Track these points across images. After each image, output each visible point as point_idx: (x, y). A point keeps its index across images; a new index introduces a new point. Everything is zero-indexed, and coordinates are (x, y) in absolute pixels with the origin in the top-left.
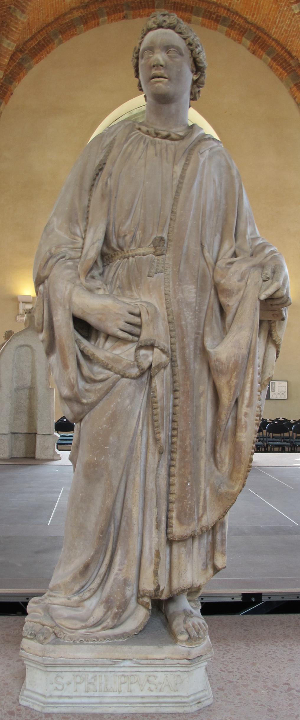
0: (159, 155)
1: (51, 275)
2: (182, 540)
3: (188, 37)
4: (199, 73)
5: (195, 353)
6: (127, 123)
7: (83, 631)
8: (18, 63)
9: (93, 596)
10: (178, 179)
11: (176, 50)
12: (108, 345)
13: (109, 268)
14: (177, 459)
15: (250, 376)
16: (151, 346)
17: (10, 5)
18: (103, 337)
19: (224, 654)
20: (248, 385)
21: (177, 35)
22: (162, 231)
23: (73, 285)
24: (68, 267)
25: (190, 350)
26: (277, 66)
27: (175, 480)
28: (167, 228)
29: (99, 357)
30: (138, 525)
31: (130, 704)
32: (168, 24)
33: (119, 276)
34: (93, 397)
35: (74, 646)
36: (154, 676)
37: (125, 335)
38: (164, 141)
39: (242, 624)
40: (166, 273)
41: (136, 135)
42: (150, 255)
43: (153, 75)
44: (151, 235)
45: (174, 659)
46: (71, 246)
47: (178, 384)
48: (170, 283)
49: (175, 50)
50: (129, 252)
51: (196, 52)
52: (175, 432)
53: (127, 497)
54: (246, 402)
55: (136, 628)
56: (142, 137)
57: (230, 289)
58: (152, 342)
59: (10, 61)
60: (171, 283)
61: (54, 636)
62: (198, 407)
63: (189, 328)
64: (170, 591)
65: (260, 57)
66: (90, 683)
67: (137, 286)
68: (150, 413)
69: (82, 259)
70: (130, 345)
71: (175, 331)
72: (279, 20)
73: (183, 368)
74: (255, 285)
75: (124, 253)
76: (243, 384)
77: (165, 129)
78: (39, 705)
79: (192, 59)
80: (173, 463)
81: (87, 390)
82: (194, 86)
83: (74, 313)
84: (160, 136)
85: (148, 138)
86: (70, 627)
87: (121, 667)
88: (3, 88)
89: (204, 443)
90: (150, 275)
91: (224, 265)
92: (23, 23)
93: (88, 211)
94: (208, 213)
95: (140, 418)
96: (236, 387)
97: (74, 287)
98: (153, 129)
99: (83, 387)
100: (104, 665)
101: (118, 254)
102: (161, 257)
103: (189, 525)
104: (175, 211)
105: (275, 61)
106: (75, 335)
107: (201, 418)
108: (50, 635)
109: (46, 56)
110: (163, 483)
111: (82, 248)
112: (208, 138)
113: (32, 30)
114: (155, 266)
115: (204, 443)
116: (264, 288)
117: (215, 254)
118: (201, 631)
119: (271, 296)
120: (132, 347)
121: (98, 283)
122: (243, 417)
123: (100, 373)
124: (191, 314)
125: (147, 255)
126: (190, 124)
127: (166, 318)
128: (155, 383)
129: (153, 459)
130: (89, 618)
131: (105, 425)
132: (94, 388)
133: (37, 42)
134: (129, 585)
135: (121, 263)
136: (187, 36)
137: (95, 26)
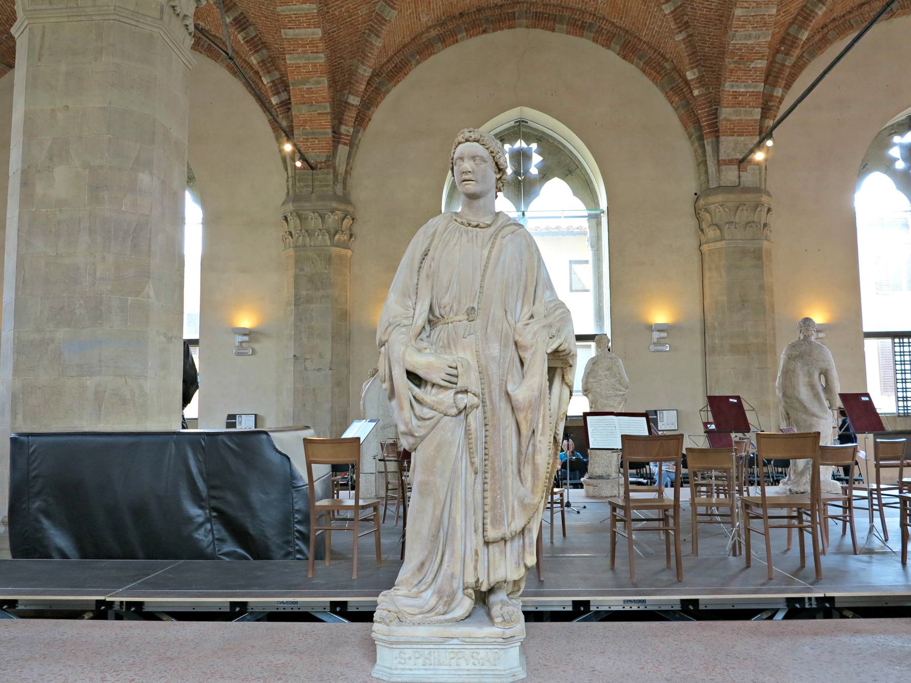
2: (495, 542)
3: (489, 147)
7: (420, 616)
8: (375, 88)
12: (434, 391)
15: (542, 412)
16: (466, 392)
20: (541, 419)
21: (481, 146)
24: (403, 333)
30: (461, 529)
31: (458, 675)
38: (474, 229)
46: (405, 316)
52: (487, 457)
54: (540, 432)
59: (366, 86)
63: (494, 377)
64: (489, 584)
66: (426, 658)
69: (413, 326)
72: (650, 23)
78: (386, 676)
81: (419, 427)
83: (408, 368)
86: (411, 613)
89: (510, 465)
91: (522, 327)
93: (417, 288)
96: (531, 421)
107: (507, 445)
110: (479, 496)
111: (413, 317)
113: (388, 53)
116: (550, 343)
121: (425, 344)
123: (426, 412)
126: (497, 210)
129: (471, 477)
133: (394, 65)
137: (454, 44)
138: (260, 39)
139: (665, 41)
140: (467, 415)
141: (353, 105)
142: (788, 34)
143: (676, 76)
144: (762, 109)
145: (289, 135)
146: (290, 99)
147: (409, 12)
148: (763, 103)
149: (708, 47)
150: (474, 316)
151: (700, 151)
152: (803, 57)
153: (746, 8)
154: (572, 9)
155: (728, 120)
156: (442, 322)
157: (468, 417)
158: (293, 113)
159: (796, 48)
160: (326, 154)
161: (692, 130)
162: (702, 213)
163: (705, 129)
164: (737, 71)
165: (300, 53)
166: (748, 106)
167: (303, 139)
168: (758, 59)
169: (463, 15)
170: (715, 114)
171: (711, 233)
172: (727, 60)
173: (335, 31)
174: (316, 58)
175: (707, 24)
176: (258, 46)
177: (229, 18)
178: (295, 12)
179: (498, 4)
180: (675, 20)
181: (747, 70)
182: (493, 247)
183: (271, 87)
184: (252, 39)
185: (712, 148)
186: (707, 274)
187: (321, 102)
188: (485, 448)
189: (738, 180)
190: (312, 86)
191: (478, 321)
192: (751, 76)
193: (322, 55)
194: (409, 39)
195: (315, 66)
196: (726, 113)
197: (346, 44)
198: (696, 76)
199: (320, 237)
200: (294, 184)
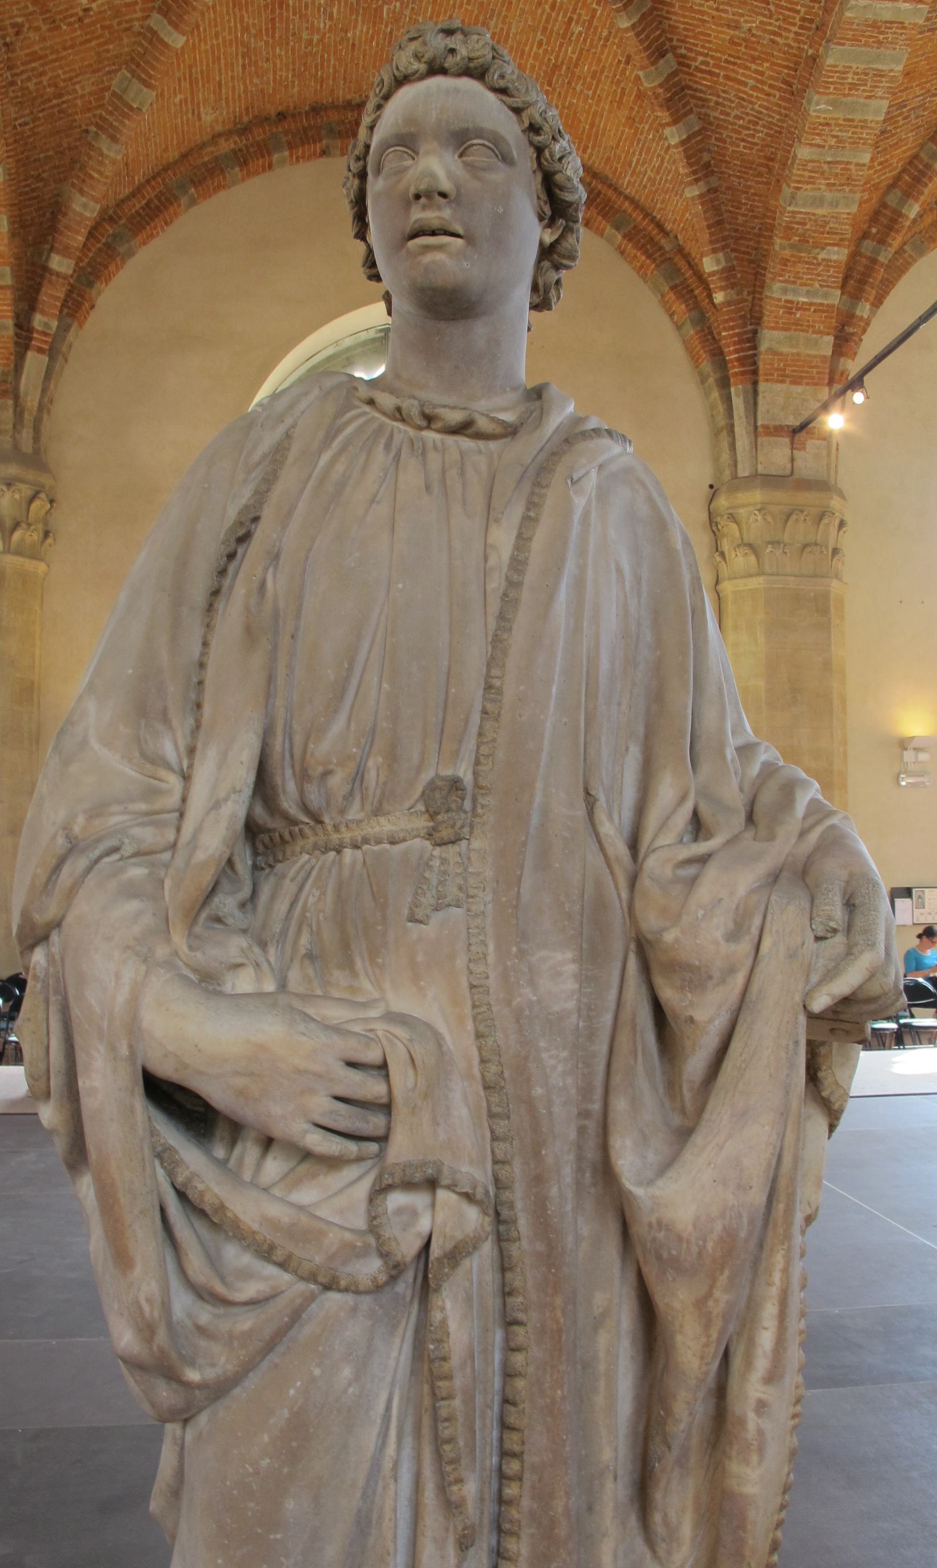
0: (436, 488)
1: (69, 919)
3: (528, 105)
4: (561, 222)
5: (578, 1185)
8: (104, 244)
10: (505, 570)
11: (490, 145)
12: (274, 1167)
13: (272, 879)
14: (521, 1559)
15: (777, 1277)
17: (87, 125)
21: (491, 97)
22: (456, 755)
23: (144, 968)
24: (130, 891)
26: (635, 251)
28: (470, 743)
29: (241, 1216)
32: (463, 59)
33: (308, 915)
34: (223, 1359)
37: (333, 1146)
38: (450, 440)
40: (474, 908)
42: (417, 843)
43: (416, 226)
44: (419, 769)
46: (143, 807)
47: (520, 1299)
48: (486, 945)
49: (486, 143)
50: (343, 829)
51: (552, 155)
54: (762, 1364)
56: (381, 427)
57: (697, 963)
58: (430, 1171)
59: (87, 239)
63: (556, 1109)
67: (373, 953)
70: (350, 1173)
71: (509, 1118)
73: (540, 1247)
74: (790, 956)
76: (750, 1299)
79: (539, 177)
81: (201, 1330)
82: (542, 264)
84: (439, 425)
85: (400, 431)
88: (74, 295)
90: (417, 917)
91: (668, 872)
92: (114, 162)
93: (201, 683)
94: (603, 680)
95: (390, 1417)
97: (147, 973)
98: (416, 403)
99: (190, 1316)
102: (451, 851)
104: (497, 683)
105: (630, 240)
107: (600, 1400)
109: (163, 230)
111: (182, 815)
112: (593, 430)
113: (133, 177)
114: (434, 883)
115: (609, 1485)
120: (360, 1178)
121: (236, 946)
122: (751, 1416)
124: (564, 1054)
125: (404, 840)
127: (476, 1071)
128: (443, 1309)
131: (268, 1460)
133: (144, 202)
135: (312, 868)
136: (524, 102)
137: (264, 170)
139: (664, 198)
141: (58, 275)
142: (884, 205)
143: (682, 264)
144: (836, 338)
147: (178, 97)
149: (744, 215)
151: (721, 408)
152: (905, 252)
153: (819, 146)
155: (775, 353)
156: (312, 839)
159: (898, 231)
161: (707, 366)
162: (723, 522)
163: (734, 367)
164: (794, 263)
166: (811, 330)
168: (834, 245)
169: (285, 118)
170: (752, 340)
171: (740, 560)
172: (778, 241)
173: (26, 124)
175: (745, 173)
179: (353, 103)
180: (688, 157)
181: (813, 264)
182: (535, 520)
185: (745, 402)
189: (789, 466)
192: (818, 275)
196: (770, 339)
197: (48, 150)
198: (721, 267)
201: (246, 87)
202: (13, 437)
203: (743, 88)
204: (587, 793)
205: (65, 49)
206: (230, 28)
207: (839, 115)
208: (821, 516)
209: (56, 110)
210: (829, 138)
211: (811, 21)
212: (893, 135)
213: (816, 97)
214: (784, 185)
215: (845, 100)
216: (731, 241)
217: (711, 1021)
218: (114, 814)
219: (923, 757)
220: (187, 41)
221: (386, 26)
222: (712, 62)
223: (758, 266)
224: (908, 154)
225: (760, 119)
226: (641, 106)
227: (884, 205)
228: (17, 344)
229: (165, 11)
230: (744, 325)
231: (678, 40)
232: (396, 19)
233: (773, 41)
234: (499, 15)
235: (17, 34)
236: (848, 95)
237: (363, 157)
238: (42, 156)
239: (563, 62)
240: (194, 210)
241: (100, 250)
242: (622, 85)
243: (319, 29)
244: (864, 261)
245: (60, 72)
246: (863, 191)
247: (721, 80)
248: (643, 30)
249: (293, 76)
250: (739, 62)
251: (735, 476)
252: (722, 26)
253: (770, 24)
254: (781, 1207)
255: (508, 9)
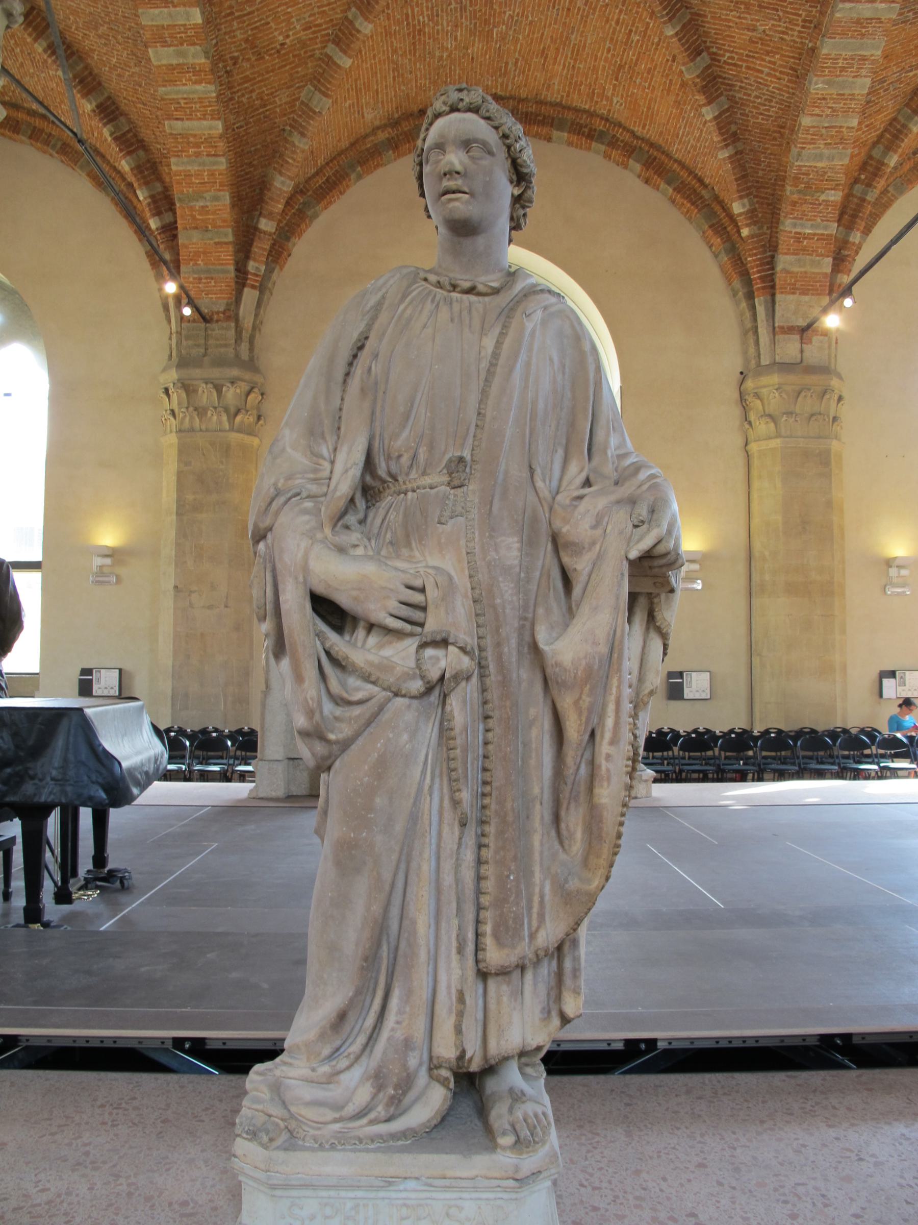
1: (276, 525)
2: (503, 973)
3: (502, 125)
4: (523, 183)
5: (520, 653)
6: (405, 271)
7: (337, 1126)
9: (356, 1065)
10: (489, 358)
12: (372, 640)
15: (614, 690)
16: (444, 643)
18: (364, 627)
19: (588, 1151)
20: (611, 707)
21: (482, 122)
22: (462, 446)
23: (310, 542)
24: (306, 512)
25: (511, 647)
27: (489, 870)
28: (470, 441)
29: (356, 661)
35: (320, 1154)
36: (457, 1207)
38: (465, 297)
39: (622, 1092)
41: (420, 289)
42: (443, 488)
44: (444, 454)
45: (492, 1178)
46: (312, 476)
53: (408, 899)
54: (608, 735)
55: (428, 1121)
56: (430, 291)
60: (477, 534)
61: (288, 1134)
62: (526, 745)
63: (507, 611)
64: (485, 1058)
65: (657, 188)
68: (445, 756)
69: (329, 497)
72: (683, 132)
73: (500, 678)
75: (399, 485)
76: (603, 704)
77: (467, 277)
79: (510, 161)
80: (485, 841)
81: (337, 719)
84: (458, 289)
86: (315, 1119)
87: (401, 1191)
88: (277, 247)
89: (538, 806)
91: (568, 502)
92: (303, 151)
93: (340, 418)
96: (590, 711)
99: (331, 713)
100: (370, 1187)
101: (388, 487)
102: (459, 490)
103: (513, 947)
104: (483, 411)
105: (679, 192)
106: (315, 624)
107: (533, 762)
108: (281, 1133)
109: (338, 198)
110: (468, 875)
111: (330, 479)
114: (451, 505)
115: (538, 806)
117: (555, 483)
118: (538, 1129)
119: (649, 551)
121: (354, 537)
122: (603, 762)
123: (359, 689)
124: (512, 585)
125: (436, 487)
128: (451, 705)
129: (451, 835)
130: (347, 1103)
132: (347, 714)
134: (413, 1049)
138: (135, 135)
140: (445, 696)
141: (265, 232)
142: (870, 157)
143: (718, 208)
144: (834, 259)
145: (175, 270)
146: (176, 222)
148: (834, 252)
149: (763, 170)
150: (463, 476)
151: (748, 314)
152: (888, 192)
153: (818, 115)
154: (577, 110)
156: (393, 489)
157: (448, 701)
158: (180, 242)
159: (881, 177)
160: (225, 301)
161: (737, 284)
162: (750, 398)
163: (757, 284)
164: (801, 204)
165: (189, 156)
167: (194, 278)
168: (832, 189)
170: (770, 263)
171: (763, 427)
172: (788, 188)
173: (241, 127)
174: (215, 164)
176: (132, 144)
177: (91, 104)
178: (185, 96)
182: (506, 334)
183: (149, 204)
184: (124, 134)
186: (756, 484)
187: (220, 227)
188: (485, 770)
189: (799, 356)
190: (208, 204)
191: (472, 487)
192: (820, 212)
193: (223, 160)
194: (347, 144)
195: (212, 174)
196: (784, 262)
197: (256, 145)
198: (746, 209)
199: (215, 418)
200: (179, 343)
201: (396, 92)
202: (235, 349)
203: (760, 75)
204: (531, 468)
205: (268, 72)
206: (384, 51)
207: (834, 91)
208: (825, 393)
209: (262, 116)
210: (826, 109)
211: (811, 22)
212: (876, 104)
213: (815, 79)
214: (793, 146)
215: (837, 79)
216: (753, 190)
217: (584, 569)
218: (298, 478)
219: (904, 572)
220: (353, 62)
221: (496, 43)
222: (736, 57)
223: (775, 207)
224: (889, 117)
225: (773, 97)
226: (684, 93)
227: (870, 157)
228: (237, 283)
229: (337, 42)
230: (765, 252)
231: (711, 42)
232: (503, 38)
233: (782, 39)
234: (578, 31)
235: (235, 64)
236: (839, 76)
237: (420, 155)
238: (253, 149)
239: (626, 63)
240: (361, 182)
241: (294, 214)
242: (670, 77)
243: (447, 49)
244: (855, 200)
245: (264, 89)
246: (853, 148)
247: (744, 70)
248: (684, 36)
249: (430, 83)
250: (756, 55)
251: (759, 364)
252: (743, 29)
253: (780, 26)
254: (616, 655)
255: (585, 26)
